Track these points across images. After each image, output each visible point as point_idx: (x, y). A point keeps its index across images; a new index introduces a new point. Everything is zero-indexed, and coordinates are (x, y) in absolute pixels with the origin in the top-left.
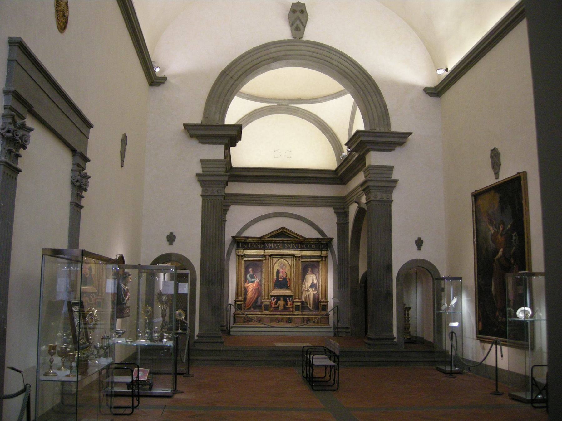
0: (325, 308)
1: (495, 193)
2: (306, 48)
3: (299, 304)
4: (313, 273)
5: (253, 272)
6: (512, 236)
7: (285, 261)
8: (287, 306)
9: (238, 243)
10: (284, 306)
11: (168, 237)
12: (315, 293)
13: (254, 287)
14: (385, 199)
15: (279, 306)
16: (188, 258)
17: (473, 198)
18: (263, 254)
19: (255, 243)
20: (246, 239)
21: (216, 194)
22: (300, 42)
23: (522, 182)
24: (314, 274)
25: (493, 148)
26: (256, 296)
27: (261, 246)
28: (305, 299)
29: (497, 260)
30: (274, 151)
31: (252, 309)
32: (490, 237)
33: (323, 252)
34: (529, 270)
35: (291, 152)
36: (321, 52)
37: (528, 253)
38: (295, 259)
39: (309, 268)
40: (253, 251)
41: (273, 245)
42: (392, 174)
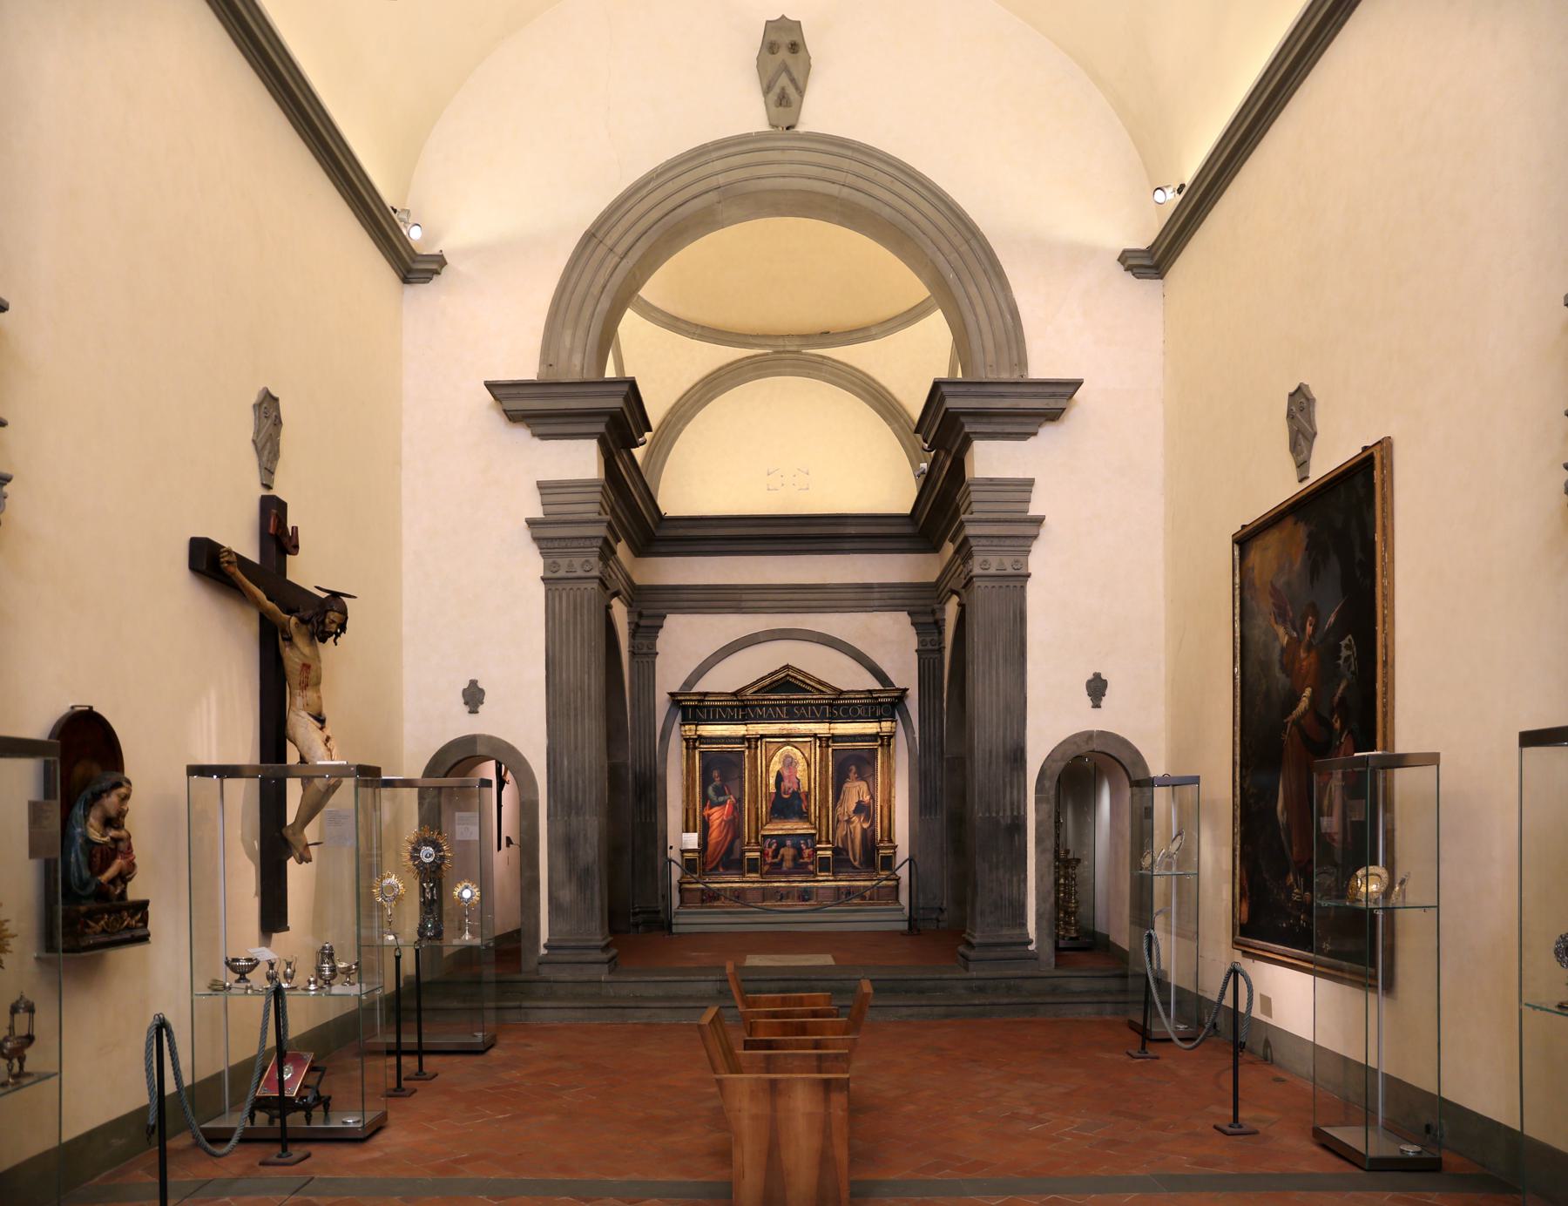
0: (888, 862)
1: (1296, 523)
2: (806, 156)
4: (861, 777)
7: (795, 750)
8: (801, 861)
9: (684, 709)
10: (795, 859)
12: (866, 826)
13: (725, 818)
14: (1010, 571)
16: (515, 746)
17: (1237, 548)
18: (744, 735)
19: (724, 708)
20: (703, 698)
21: (580, 573)
23: (1377, 474)
24: (863, 779)
25: (1296, 387)
26: (729, 838)
31: (721, 870)
32: (1276, 656)
33: (883, 724)
34: (1385, 748)
36: (845, 164)
37: (1385, 693)
38: (818, 744)
42: (1028, 501)
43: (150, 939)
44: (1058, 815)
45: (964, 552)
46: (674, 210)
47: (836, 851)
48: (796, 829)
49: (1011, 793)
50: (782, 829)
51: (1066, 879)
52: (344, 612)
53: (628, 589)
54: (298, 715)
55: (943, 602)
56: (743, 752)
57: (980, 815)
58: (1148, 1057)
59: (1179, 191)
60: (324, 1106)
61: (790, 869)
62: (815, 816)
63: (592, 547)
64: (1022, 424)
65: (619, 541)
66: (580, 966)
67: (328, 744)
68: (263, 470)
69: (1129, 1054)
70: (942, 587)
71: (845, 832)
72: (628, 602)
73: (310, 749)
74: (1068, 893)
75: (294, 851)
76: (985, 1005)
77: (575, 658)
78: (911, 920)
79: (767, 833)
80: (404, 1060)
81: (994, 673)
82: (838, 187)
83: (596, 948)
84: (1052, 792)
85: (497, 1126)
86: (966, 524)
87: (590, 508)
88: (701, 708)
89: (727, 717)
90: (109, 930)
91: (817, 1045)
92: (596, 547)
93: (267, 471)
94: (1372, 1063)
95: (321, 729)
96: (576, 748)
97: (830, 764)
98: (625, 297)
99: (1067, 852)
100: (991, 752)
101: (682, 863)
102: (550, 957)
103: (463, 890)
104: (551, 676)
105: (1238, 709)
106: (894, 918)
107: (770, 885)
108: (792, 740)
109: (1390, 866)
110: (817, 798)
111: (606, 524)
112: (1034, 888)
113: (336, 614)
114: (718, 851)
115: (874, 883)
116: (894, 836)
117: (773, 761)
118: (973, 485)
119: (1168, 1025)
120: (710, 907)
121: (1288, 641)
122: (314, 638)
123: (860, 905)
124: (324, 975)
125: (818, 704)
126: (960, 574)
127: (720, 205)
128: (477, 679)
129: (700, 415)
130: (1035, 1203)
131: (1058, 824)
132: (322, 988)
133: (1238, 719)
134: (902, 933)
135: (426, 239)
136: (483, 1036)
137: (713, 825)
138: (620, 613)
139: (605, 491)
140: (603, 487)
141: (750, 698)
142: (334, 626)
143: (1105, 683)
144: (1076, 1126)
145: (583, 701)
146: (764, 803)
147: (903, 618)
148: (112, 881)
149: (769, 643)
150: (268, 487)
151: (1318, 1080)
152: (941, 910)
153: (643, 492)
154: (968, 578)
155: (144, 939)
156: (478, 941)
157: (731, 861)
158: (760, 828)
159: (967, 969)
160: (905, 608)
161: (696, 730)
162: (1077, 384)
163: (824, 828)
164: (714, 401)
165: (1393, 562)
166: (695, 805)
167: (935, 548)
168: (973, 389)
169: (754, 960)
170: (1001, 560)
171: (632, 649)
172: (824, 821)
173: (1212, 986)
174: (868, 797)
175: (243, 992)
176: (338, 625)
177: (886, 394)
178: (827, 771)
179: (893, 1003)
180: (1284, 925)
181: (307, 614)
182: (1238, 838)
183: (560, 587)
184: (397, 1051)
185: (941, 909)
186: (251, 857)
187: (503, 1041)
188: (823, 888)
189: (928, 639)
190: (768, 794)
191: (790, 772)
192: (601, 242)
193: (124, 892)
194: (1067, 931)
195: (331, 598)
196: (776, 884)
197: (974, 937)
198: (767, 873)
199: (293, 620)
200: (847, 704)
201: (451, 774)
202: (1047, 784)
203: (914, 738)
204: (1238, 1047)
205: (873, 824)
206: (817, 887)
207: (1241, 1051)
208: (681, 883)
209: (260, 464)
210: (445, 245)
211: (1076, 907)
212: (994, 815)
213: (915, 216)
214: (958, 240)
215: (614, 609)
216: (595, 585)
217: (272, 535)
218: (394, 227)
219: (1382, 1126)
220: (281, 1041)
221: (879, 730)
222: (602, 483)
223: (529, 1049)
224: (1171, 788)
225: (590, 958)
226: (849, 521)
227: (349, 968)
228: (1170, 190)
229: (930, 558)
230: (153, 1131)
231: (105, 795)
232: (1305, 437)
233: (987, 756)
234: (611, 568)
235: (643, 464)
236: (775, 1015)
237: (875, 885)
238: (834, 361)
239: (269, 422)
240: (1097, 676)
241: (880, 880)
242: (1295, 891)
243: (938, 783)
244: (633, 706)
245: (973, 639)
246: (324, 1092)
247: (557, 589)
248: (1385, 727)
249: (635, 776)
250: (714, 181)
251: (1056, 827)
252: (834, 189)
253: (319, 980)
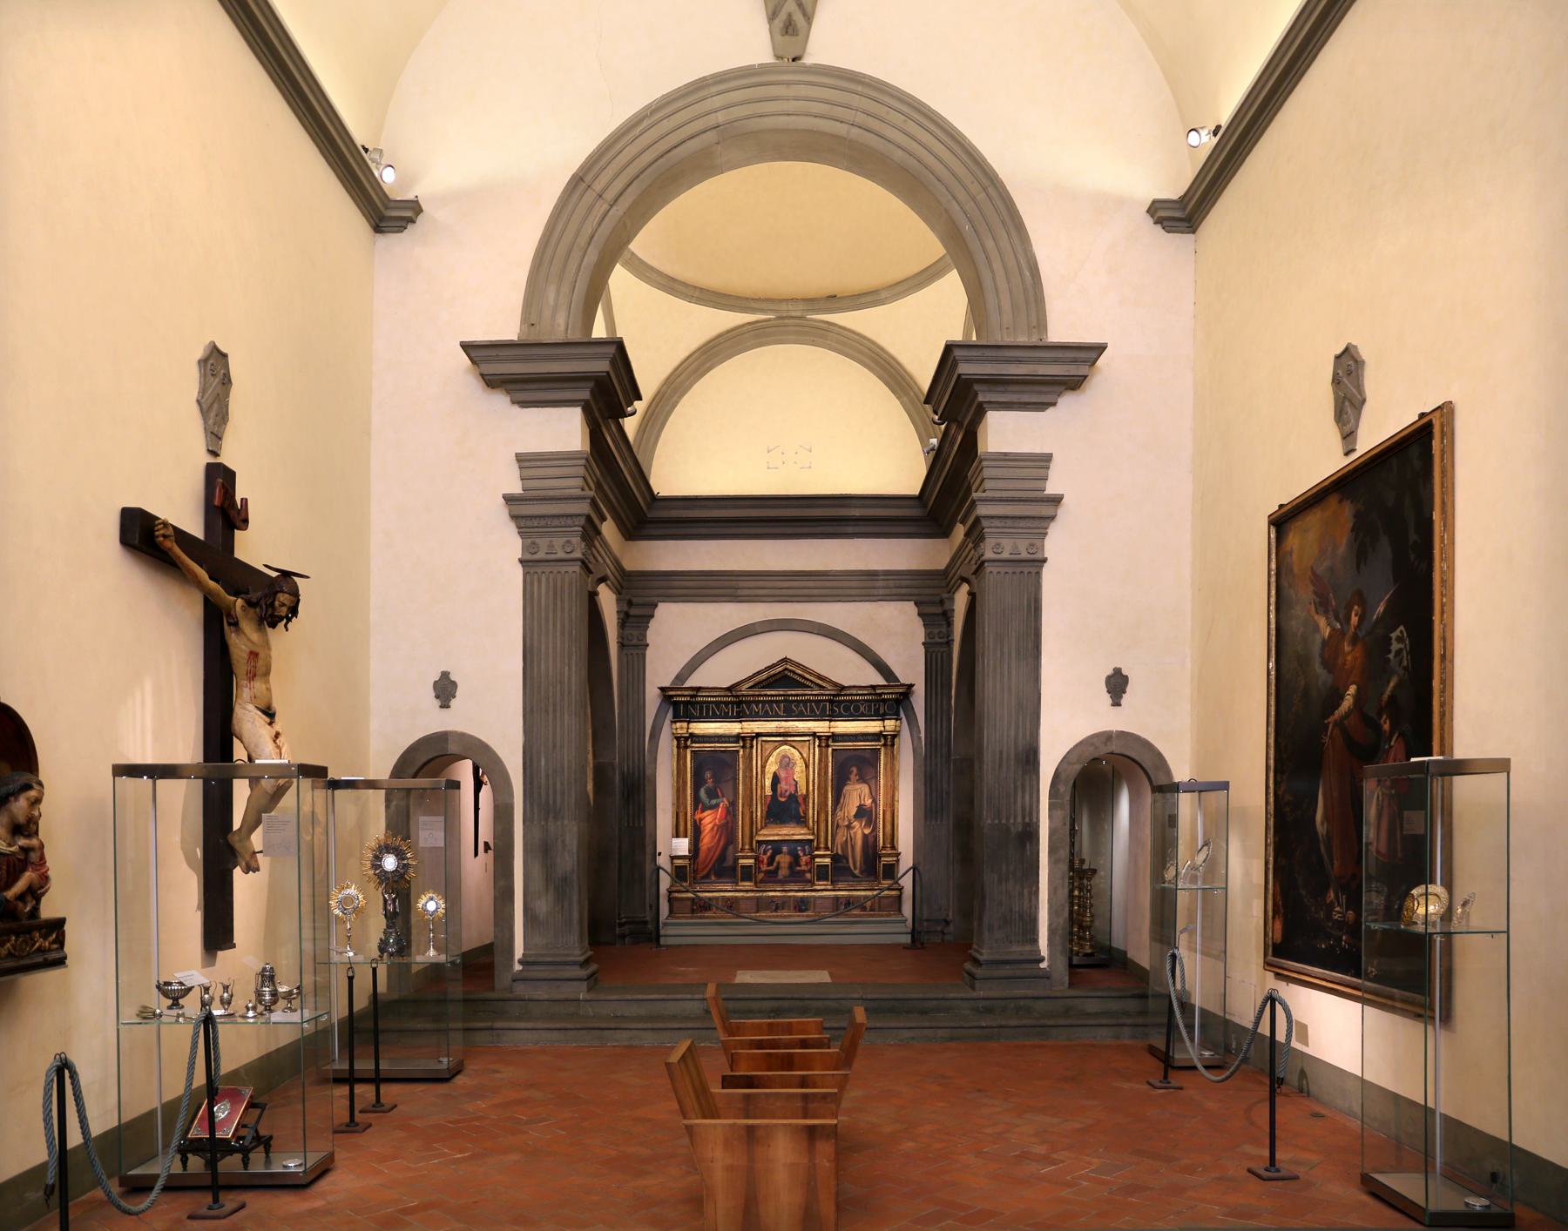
0: (891, 871)
1: (1340, 501)
3: (827, 861)
4: (862, 779)
6: (1391, 638)
8: (798, 868)
9: (676, 705)
10: (791, 866)
12: (867, 831)
13: (717, 821)
14: (1024, 555)
15: (778, 867)
17: (1273, 530)
18: (739, 734)
19: (718, 704)
21: (561, 555)
22: (794, 72)
23: (1436, 444)
29: (1336, 724)
31: (713, 878)
32: (1316, 649)
33: (887, 722)
35: (810, 451)
36: (855, 100)
37: (1443, 691)
38: (817, 744)
39: (852, 767)
41: (763, 709)
43: (67, 961)
45: (976, 533)
46: (669, 151)
47: (835, 858)
48: (793, 835)
49: (1023, 797)
51: (1081, 890)
52: (295, 594)
53: (617, 574)
55: (952, 591)
56: (738, 751)
57: (989, 821)
59: (1215, 134)
60: (265, 1147)
61: (785, 877)
62: (813, 821)
64: (1040, 393)
65: (603, 519)
66: (558, 983)
67: (278, 741)
68: (209, 435)
71: (845, 839)
72: (617, 589)
73: (256, 746)
74: (1083, 906)
75: (240, 859)
76: (992, 1027)
77: (555, 648)
78: (913, 933)
80: (359, 1089)
81: (1006, 667)
82: (845, 127)
83: (574, 963)
84: (1068, 798)
85: (453, 1167)
86: (977, 503)
87: (573, 484)
88: (693, 704)
89: (721, 714)
90: (17, 954)
93: (213, 437)
94: (1431, 1104)
95: (270, 724)
96: (554, 746)
97: (830, 764)
98: (613, 250)
99: (1082, 861)
100: (1001, 753)
101: (672, 871)
102: (525, 974)
104: (528, 670)
105: (1273, 709)
106: (897, 930)
107: (765, 894)
108: (789, 739)
109: (1448, 885)
111: (589, 501)
113: (287, 596)
114: (709, 858)
115: (875, 893)
116: (897, 842)
117: (769, 761)
119: (1192, 1051)
120: (701, 918)
121: (1330, 633)
123: (860, 916)
124: (264, 1000)
125: (818, 701)
127: (719, 146)
131: (1073, 832)
132: (261, 1014)
133: (1272, 719)
134: (905, 947)
136: (449, 1061)
138: (608, 600)
139: (590, 465)
140: (587, 460)
142: (284, 609)
143: (1125, 680)
144: (1093, 1168)
145: (562, 695)
147: (910, 608)
148: (21, 897)
149: (767, 634)
150: (215, 454)
151: (1365, 1119)
152: (947, 923)
154: (979, 562)
155: (61, 962)
156: (443, 958)
157: (724, 869)
159: (973, 988)
160: (911, 598)
162: (1100, 349)
163: (823, 834)
164: (711, 372)
165: (1453, 544)
166: (686, 808)
167: (944, 532)
168: (988, 353)
169: (745, 977)
170: (1015, 543)
173: (1244, 1011)
174: (870, 801)
175: (174, 1019)
176: (289, 608)
177: (896, 365)
178: (826, 773)
179: (892, 1025)
180: (1323, 946)
181: (254, 596)
182: (1271, 849)
183: (539, 571)
184: (349, 1079)
186: (189, 864)
187: (471, 1066)
189: (936, 631)
190: (763, 796)
193: (35, 911)
194: (1082, 946)
195: (282, 578)
197: (981, 954)
198: (762, 881)
199: (240, 602)
200: (849, 701)
201: (421, 774)
202: (1062, 789)
203: (920, 738)
204: (1276, 1083)
205: (875, 829)
206: (814, 897)
208: (670, 892)
209: (205, 429)
211: (1092, 921)
212: (1004, 821)
213: (930, 160)
214: (974, 188)
215: (600, 596)
216: (577, 568)
217: (217, 507)
218: (364, 168)
219: (1441, 1174)
220: (212, 1081)
221: (882, 729)
223: (498, 1075)
224: (1196, 794)
225: (567, 975)
226: (854, 502)
227: (290, 992)
228: (1206, 131)
230: (52, 1192)
231: (12, 799)
232: (1352, 405)
233: (998, 756)
234: (596, 549)
235: (635, 441)
237: (877, 895)
238: (841, 327)
239: (217, 380)
240: (1118, 671)
241: (882, 890)
242: (1337, 909)
243: (945, 786)
244: (621, 701)
245: (984, 628)
246: (263, 1132)
248: (1442, 729)
249: (622, 774)
250: (712, 120)
251: (1070, 834)
252: (841, 129)
253: (259, 1005)
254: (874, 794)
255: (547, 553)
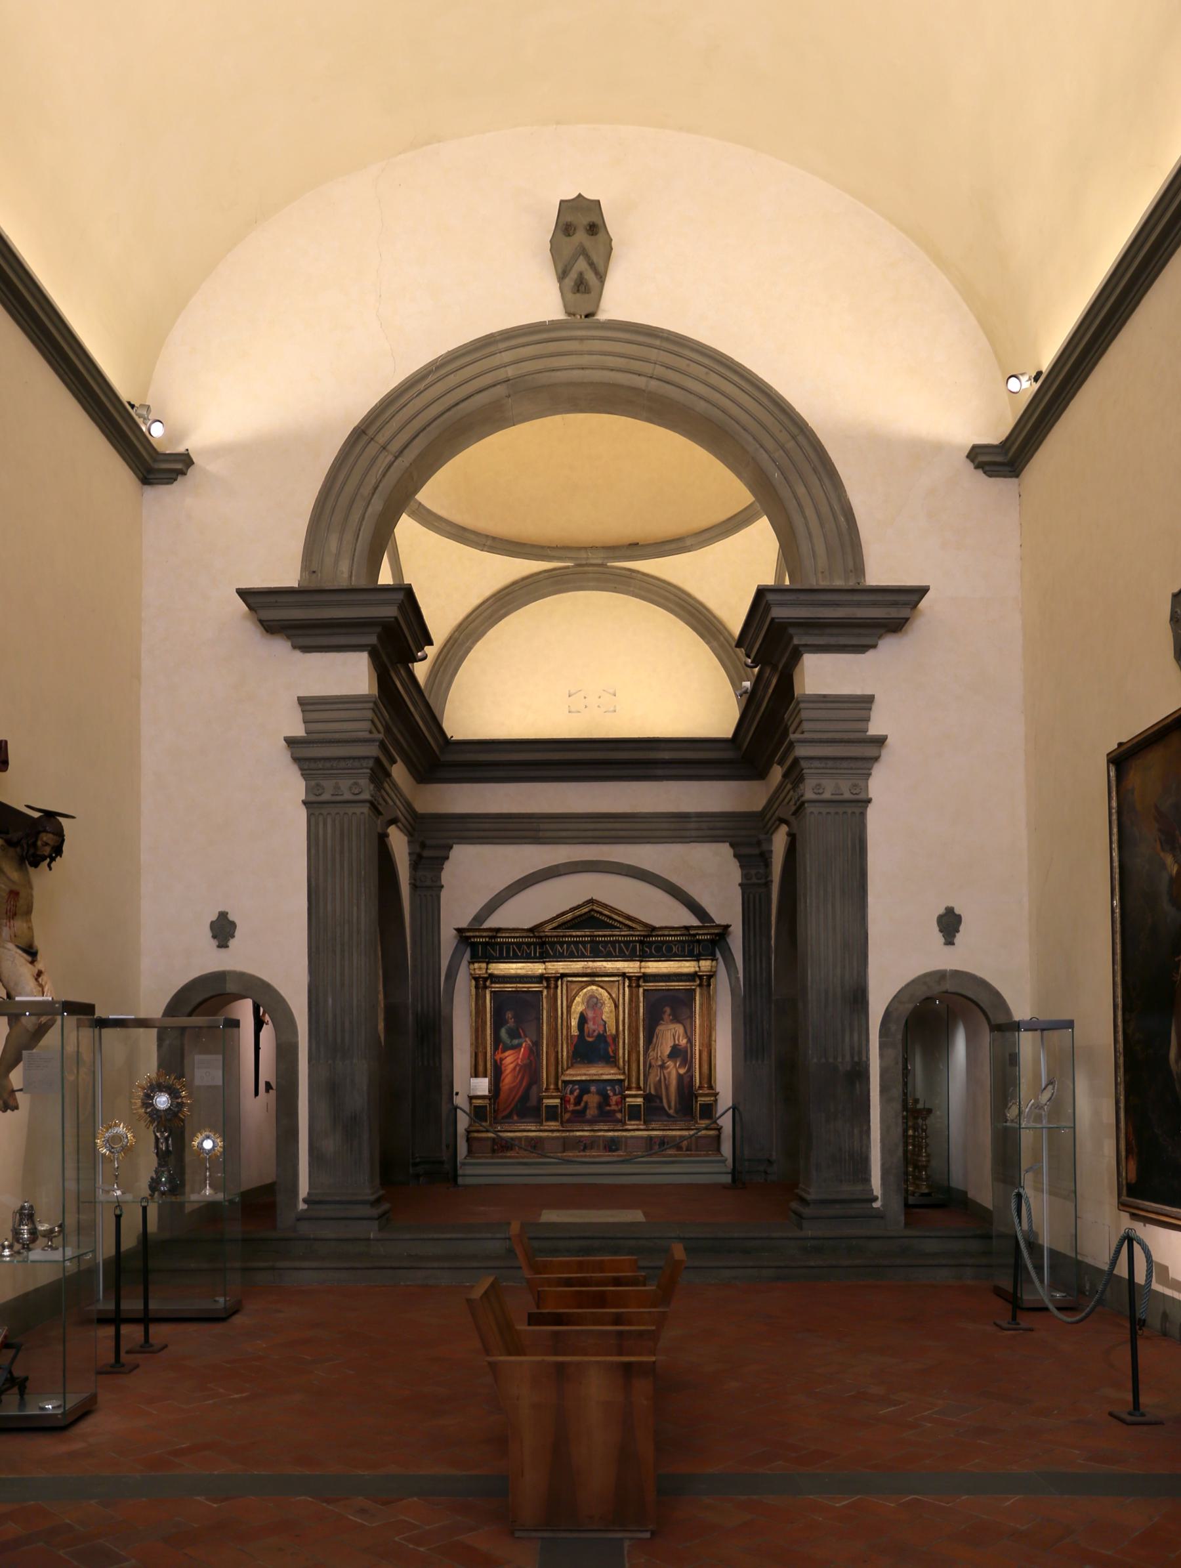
0: (708, 1111)
3: (640, 1101)
4: (676, 1019)
5: (515, 1022)
7: (600, 989)
8: (608, 1108)
9: (473, 946)
10: (600, 1106)
11: (213, 925)
12: (682, 1071)
14: (847, 795)
15: (586, 1107)
19: (519, 945)
21: (347, 796)
22: (588, 328)
24: (679, 1022)
26: (524, 1084)
27: (535, 953)
28: (656, 1089)
30: (569, 696)
31: (515, 1118)
33: (702, 963)
36: (653, 354)
38: (627, 984)
40: (514, 966)
42: (868, 720)
44: (905, 1061)
47: (648, 1098)
48: (602, 1074)
50: (585, 1075)
51: (915, 1130)
52: (60, 834)
54: (5, 948)
55: (770, 832)
56: (541, 992)
58: (1020, 1329)
60: (19, 1389)
63: (361, 769)
65: (394, 762)
67: (40, 980)
69: (997, 1325)
70: (768, 817)
71: (658, 1078)
74: (918, 1147)
78: (734, 1173)
79: (568, 1078)
80: (125, 1329)
82: (644, 379)
83: (364, 1202)
84: (900, 1037)
86: (795, 744)
89: (522, 954)
91: (618, 1320)
92: (367, 768)
95: (32, 962)
97: (641, 1005)
103: (203, 1141)
107: (572, 1134)
108: (597, 979)
110: (626, 1041)
112: (879, 1141)
113: (51, 836)
115: (692, 1132)
116: (715, 1081)
118: (803, 702)
119: (1041, 1291)
120: (502, 1157)
121: (1177, 871)
122: (25, 863)
123: (676, 1156)
124: (22, 1239)
126: (788, 803)
128: (227, 910)
129: (491, 633)
130: (893, 1505)
131: (906, 1072)
132: (19, 1253)
133: (1118, 957)
134: (724, 1187)
135: (169, 436)
136: (225, 1301)
137: (505, 1070)
138: (399, 843)
140: (375, 703)
141: (549, 934)
143: (958, 919)
144: (936, 1409)
146: (565, 1046)
147: (725, 850)
152: (770, 1162)
153: (425, 713)
154: (798, 803)
156: (220, 1197)
157: (528, 1108)
158: (560, 1074)
159: (801, 1228)
161: (487, 969)
162: (922, 591)
163: (634, 1074)
166: (485, 1048)
167: (761, 774)
168: (803, 597)
169: (550, 1216)
171: (413, 881)
172: (634, 1066)
174: (685, 1041)
178: (637, 1012)
181: (15, 836)
182: (1121, 1088)
184: (116, 1319)
185: (769, 1161)
188: (632, 1137)
189: (753, 872)
191: (594, 1013)
192: (372, 439)
194: (918, 1186)
196: (578, 1134)
197: (808, 1193)
198: (569, 1121)
200: (661, 941)
202: (893, 1027)
203: (738, 978)
204: (1137, 1324)
205: (690, 1069)
207: (1140, 1329)
208: (468, 1132)
210: (191, 444)
212: (831, 1060)
214: (783, 437)
216: (365, 809)
221: (697, 969)
222: (374, 699)
224: (1038, 1033)
227: (51, 1231)
229: (755, 785)
236: (568, 1282)
237: (693, 1135)
240: (950, 911)
241: (699, 1130)
246: (17, 1373)
247: (321, 814)
250: (501, 374)
252: (640, 382)
253: (16, 1244)
254: (689, 1034)
255: (333, 795)
